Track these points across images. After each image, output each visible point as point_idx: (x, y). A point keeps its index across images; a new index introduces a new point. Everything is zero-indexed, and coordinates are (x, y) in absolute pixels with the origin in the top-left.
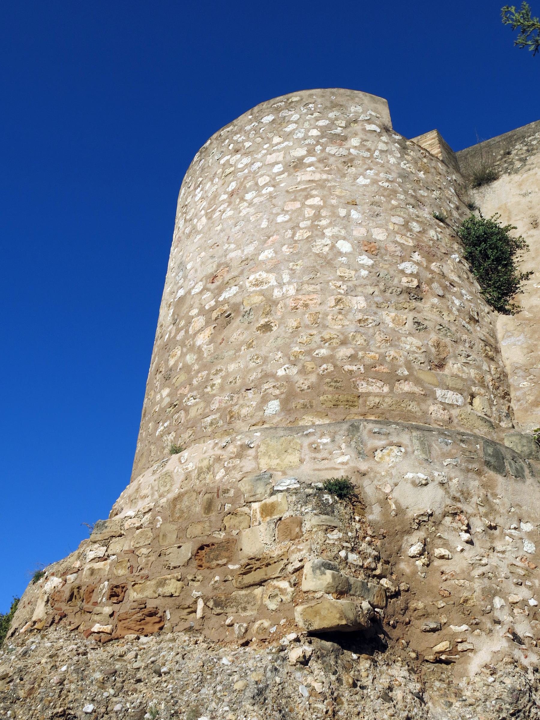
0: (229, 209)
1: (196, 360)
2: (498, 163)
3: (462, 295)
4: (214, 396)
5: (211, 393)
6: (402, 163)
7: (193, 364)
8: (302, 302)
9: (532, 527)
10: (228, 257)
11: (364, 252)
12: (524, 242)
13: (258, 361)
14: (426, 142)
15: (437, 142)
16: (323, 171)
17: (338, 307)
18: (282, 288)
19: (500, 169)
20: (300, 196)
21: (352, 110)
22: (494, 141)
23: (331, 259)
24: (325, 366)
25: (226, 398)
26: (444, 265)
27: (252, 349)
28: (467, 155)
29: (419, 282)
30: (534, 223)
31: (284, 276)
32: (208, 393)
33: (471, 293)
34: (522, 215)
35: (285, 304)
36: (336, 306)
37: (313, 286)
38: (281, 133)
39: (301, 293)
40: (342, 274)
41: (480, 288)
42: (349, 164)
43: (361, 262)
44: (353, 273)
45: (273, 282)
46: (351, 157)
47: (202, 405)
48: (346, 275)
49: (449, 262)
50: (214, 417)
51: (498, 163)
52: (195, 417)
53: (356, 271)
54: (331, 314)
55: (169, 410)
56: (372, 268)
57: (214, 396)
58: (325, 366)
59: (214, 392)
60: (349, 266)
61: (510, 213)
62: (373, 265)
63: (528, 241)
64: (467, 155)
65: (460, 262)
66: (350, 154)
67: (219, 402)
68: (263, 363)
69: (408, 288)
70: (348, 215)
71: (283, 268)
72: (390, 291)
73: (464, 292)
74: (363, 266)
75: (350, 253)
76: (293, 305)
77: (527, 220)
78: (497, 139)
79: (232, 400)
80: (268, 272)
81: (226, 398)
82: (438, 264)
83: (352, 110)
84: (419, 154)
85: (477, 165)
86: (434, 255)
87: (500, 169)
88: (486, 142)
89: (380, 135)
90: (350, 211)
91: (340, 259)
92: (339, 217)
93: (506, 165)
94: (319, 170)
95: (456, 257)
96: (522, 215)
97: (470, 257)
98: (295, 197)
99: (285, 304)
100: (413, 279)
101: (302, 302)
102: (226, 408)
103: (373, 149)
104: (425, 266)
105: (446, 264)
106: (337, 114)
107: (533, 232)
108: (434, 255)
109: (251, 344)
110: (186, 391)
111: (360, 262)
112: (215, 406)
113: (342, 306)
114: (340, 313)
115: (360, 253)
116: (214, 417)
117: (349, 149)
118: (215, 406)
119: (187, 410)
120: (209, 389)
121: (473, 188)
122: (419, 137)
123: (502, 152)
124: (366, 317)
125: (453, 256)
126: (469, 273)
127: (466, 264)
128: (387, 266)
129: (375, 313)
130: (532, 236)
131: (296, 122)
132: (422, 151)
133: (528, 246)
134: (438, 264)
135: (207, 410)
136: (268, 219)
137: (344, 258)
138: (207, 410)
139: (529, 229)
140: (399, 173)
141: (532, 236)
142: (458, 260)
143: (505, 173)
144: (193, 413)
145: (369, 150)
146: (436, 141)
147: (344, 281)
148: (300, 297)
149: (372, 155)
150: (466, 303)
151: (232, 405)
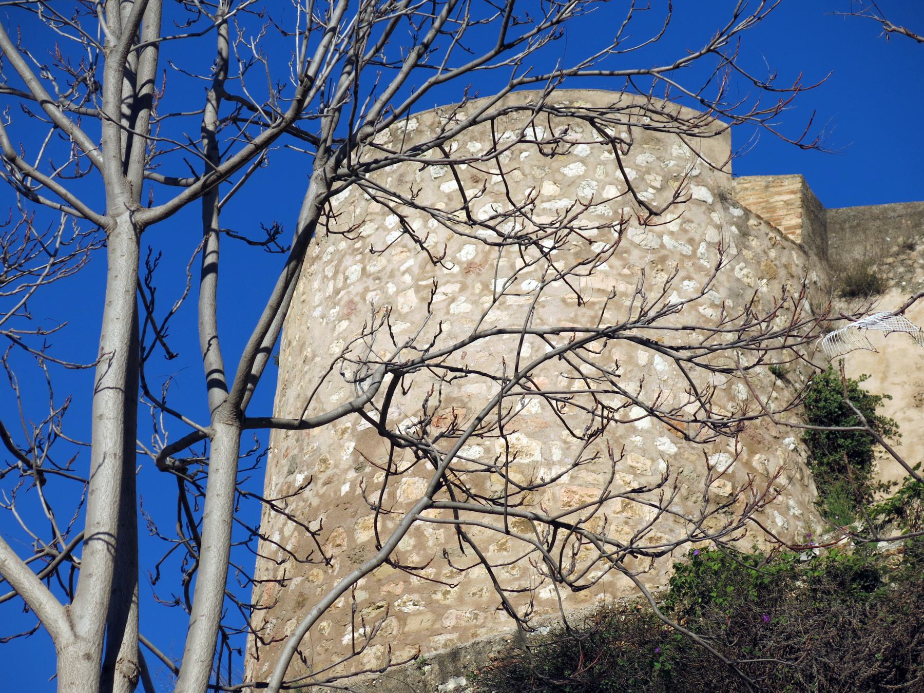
0: (463, 298)
1: (415, 547)
2: (890, 260)
3: (788, 508)
4: (448, 607)
5: (443, 602)
6: (737, 267)
7: (411, 552)
8: (577, 497)
9: (639, 351)
10: (463, 389)
11: (666, 431)
12: (897, 426)
13: (514, 572)
14: (780, 194)
15: (799, 203)
16: (620, 275)
17: (625, 514)
18: (550, 469)
19: (891, 275)
20: (583, 316)
21: (675, 153)
22: (894, 211)
23: (621, 436)
24: (602, 596)
25: (468, 615)
26: (772, 459)
27: (505, 553)
28: (845, 221)
29: (734, 488)
30: (918, 398)
31: (554, 450)
32: (437, 601)
33: (801, 504)
34: (904, 378)
35: (554, 495)
36: (622, 511)
37: (594, 476)
38: (558, 177)
39: (576, 483)
40: (634, 464)
41: (816, 493)
42: (660, 267)
43: (661, 448)
44: (649, 463)
45: (538, 457)
46: (664, 252)
47: (429, 616)
48: (639, 465)
49: (779, 453)
50: (449, 636)
51: (890, 260)
52: (418, 632)
53: (653, 460)
54: (614, 524)
55: (367, 610)
56: (675, 459)
57: (448, 607)
58: (602, 596)
59: (447, 602)
60: (644, 452)
61: (887, 366)
62: (676, 454)
63: (904, 428)
64: (845, 221)
65: (795, 450)
66: (663, 246)
67: (457, 618)
68: (521, 576)
69: (718, 496)
70: (651, 362)
71: (552, 436)
72: (694, 499)
73: (791, 503)
74: (662, 455)
75: (647, 431)
76: (565, 499)
77: (910, 390)
78: (900, 207)
79: (476, 619)
80: (530, 435)
81: (468, 615)
82: (764, 457)
83: (675, 153)
84: (767, 243)
85: (854, 253)
86: (760, 442)
87: (891, 275)
88: (881, 206)
89: (711, 209)
90: (653, 357)
91: (633, 439)
92: (637, 365)
93: (901, 270)
94: (615, 272)
95: (790, 441)
96: (904, 378)
97: (811, 440)
98: (576, 315)
99: (554, 495)
100: (727, 482)
101: (577, 497)
102: (466, 629)
103: (697, 238)
104: (744, 461)
105: (775, 456)
106: (650, 160)
107: (913, 413)
108: (760, 442)
109: (504, 544)
110: (399, 589)
111: (659, 448)
112: (449, 622)
113: (630, 514)
114: (626, 523)
115: (660, 433)
116: (449, 636)
117: (660, 236)
118: (449, 622)
119: (403, 618)
120: (439, 596)
121: (840, 297)
122: (770, 178)
123: (901, 240)
124: (659, 535)
125: (787, 441)
126: (804, 467)
127: (803, 454)
128: (693, 458)
129: (672, 530)
130: (910, 420)
131: (583, 161)
132: (771, 235)
133: (900, 436)
134: (764, 457)
135: (437, 626)
136: (532, 343)
137: (638, 438)
138: (437, 626)
139: (909, 406)
140: (730, 289)
141: (910, 420)
142: (792, 447)
143: (898, 284)
144: (413, 625)
145: (691, 241)
146: (796, 198)
147: (635, 475)
148: (575, 488)
149: (694, 252)
150: (792, 521)
151: (476, 627)
